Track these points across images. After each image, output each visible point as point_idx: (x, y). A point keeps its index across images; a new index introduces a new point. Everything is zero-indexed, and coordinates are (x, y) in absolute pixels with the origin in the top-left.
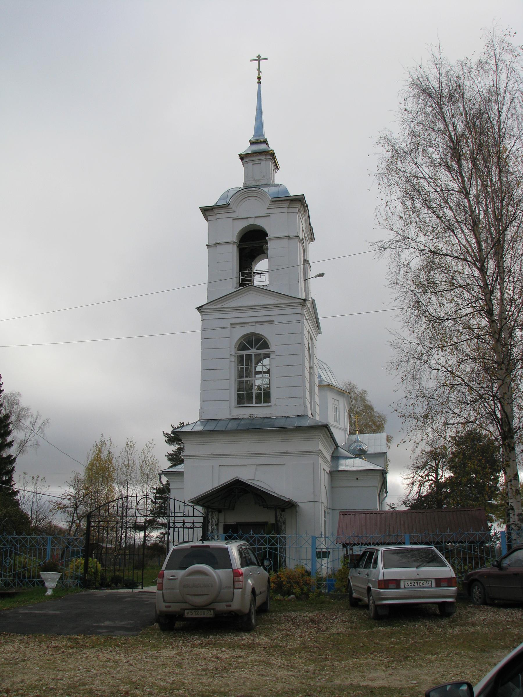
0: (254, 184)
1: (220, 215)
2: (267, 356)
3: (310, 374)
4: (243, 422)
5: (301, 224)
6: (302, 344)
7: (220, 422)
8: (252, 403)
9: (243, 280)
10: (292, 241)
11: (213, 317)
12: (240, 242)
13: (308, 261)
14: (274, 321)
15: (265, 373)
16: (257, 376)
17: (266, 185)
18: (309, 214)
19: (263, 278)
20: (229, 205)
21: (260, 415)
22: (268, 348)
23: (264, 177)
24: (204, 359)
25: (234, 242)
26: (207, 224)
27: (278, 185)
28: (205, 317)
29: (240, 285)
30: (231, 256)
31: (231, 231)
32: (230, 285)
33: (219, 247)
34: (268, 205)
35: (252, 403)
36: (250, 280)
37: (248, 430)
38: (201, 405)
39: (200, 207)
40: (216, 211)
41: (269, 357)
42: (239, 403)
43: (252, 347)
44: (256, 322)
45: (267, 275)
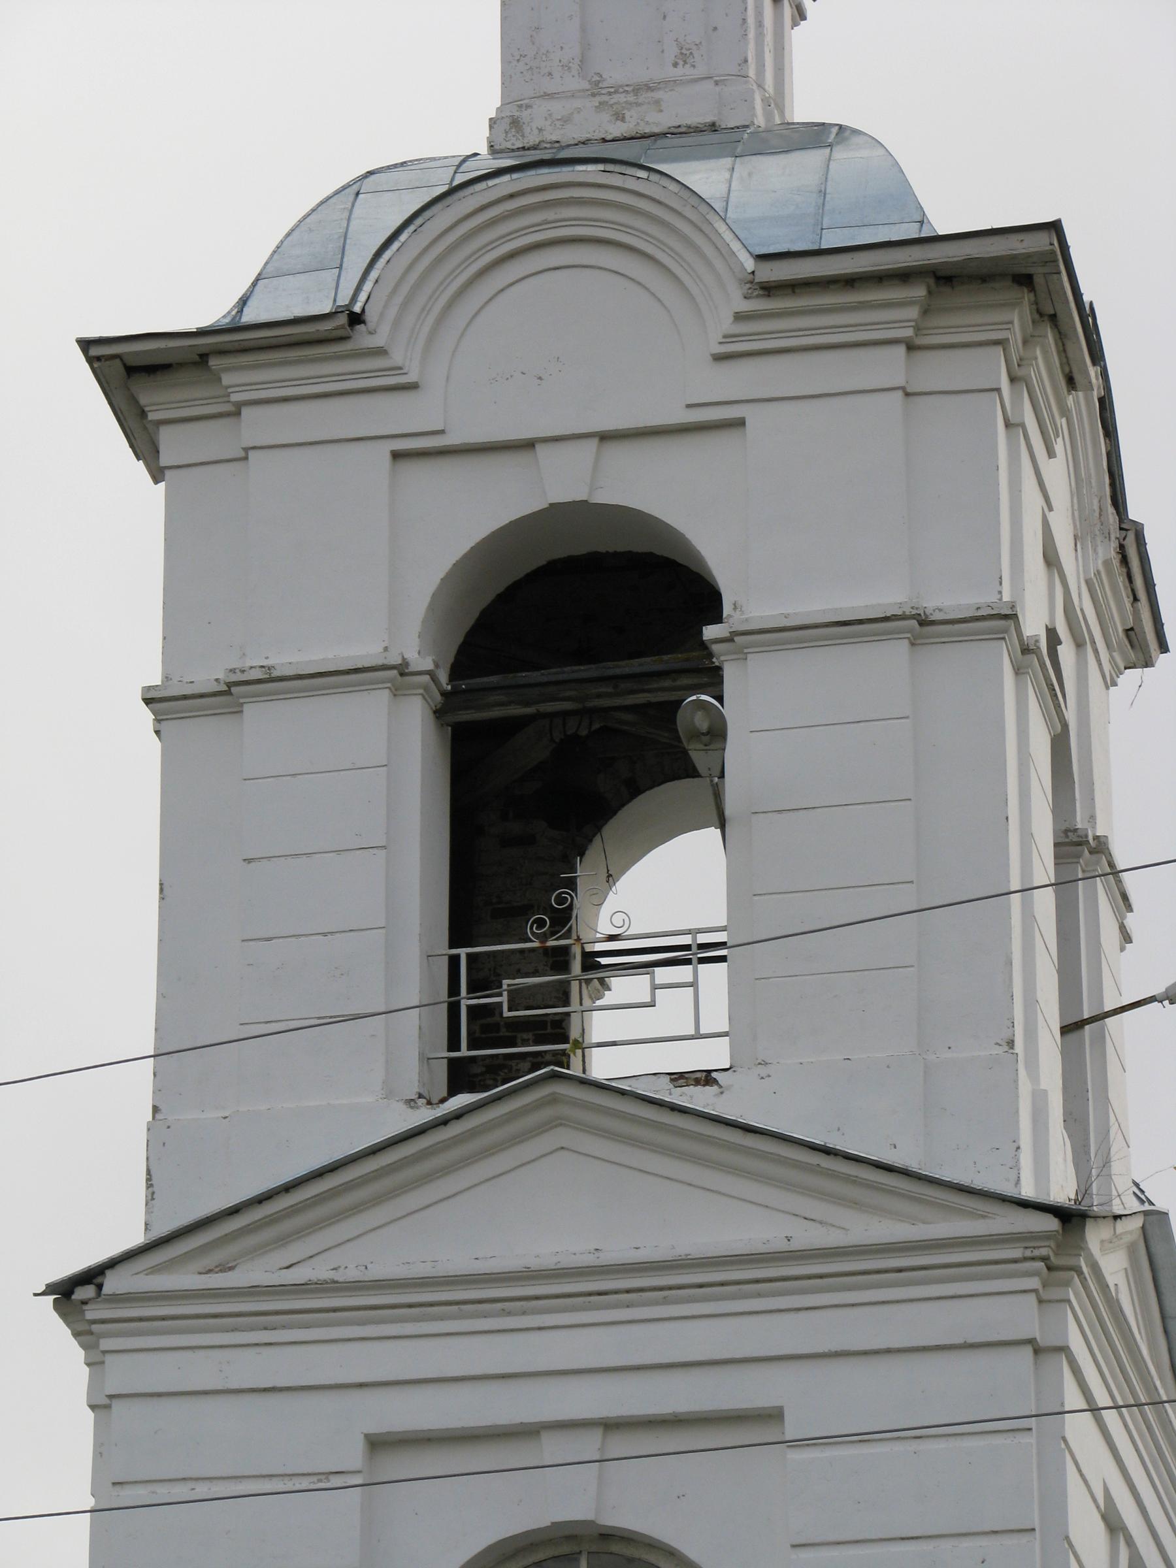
0: (590, 123)
1: (277, 416)
5: (1042, 494)
9: (488, 1029)
10: (952, 662)
11: (202, 1370)
12: (456, 672)
13: (1101, 847)
14: (773, 1416)
17: (711, 137)
18: (1106, 405)
19: (673, 1013)
20: (356, 319)
23: (684, 57)
25: (403, 669)
26: (151, 497)
27: (820, 136)
28: (126, 1373)
29: (461, 1077)
30: (375, 795)
31: (381, 574)
32: (371, 1076)
33: (258, 715)
34: (727, 324)
36: (557, 1030)
39: (86, 345)
40: (238, 379)
44: (611, 1426)
45: (714, 976)
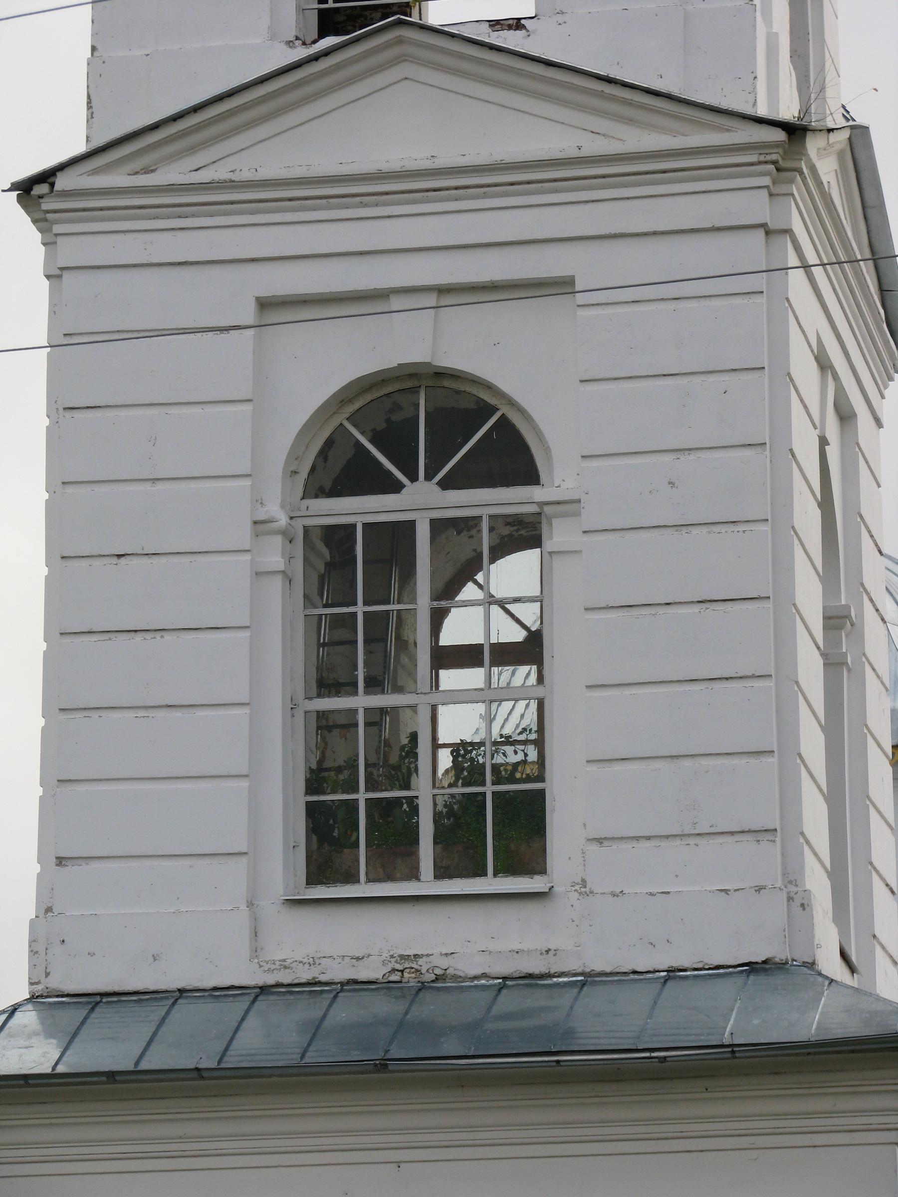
2: (521, 533)
3: (834, 665)
4: (345, 1012)
6: (772, 446)
7: (184, 1009)
8: (414, 875)
11: (131, 249)
15: (505, 655)
16: (451, 679)
21: (469, 965)
22: (529, 475)
24: (62, 556)
28: (73, 251)
35: (414, 875)
37: (382, 1066)
38: (45, 888)
41: (533, 541)
42: (313, 879)
43: (414, 469)
44: (442, 290)
